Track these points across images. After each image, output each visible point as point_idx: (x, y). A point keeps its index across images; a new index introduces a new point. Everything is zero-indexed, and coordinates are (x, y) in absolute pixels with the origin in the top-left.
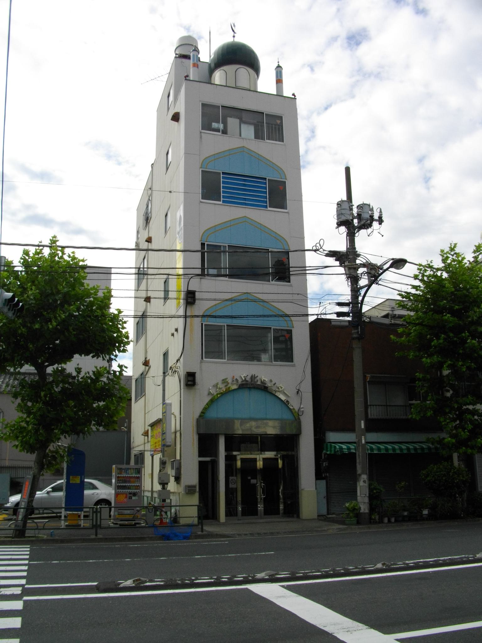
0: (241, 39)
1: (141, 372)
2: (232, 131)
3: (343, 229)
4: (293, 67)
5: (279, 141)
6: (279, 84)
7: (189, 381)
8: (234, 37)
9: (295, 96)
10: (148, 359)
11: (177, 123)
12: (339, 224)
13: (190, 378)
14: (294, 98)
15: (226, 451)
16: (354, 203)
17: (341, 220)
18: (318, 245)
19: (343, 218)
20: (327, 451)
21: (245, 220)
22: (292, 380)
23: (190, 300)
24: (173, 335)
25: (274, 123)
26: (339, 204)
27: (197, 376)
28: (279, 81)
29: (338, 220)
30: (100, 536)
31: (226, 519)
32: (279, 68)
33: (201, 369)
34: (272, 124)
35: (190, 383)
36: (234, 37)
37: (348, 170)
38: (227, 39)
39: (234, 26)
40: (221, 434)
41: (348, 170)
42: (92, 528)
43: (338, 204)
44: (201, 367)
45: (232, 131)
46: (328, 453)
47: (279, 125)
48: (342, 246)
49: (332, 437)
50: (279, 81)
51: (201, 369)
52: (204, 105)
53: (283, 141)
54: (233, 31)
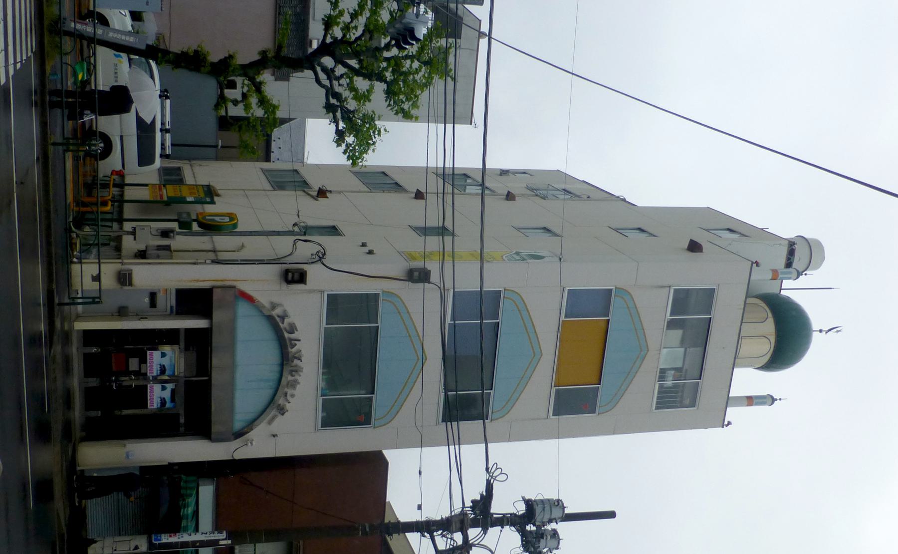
0: (817, 339)
1: (310, 180)
2: (695, 317)
3: (521, 508)
4: (774, 422)
5: (657, 403)
6: (746, 402)
7: (293, 274)
8: (821, 331)
9: (727, 426)
10: (328, 195)
11: (686, 246)
12: (529, 504)
13: (297, 276)
14: (724, 424)
15: (186, 329)
16: (560, 524)
17: (536, 507)
18: (499, 471)
19: (538, 509)
20: (186, 482)
21: (536, 354)
22: (297, 431)
23: (416, 274)
24: (364, 245)
25: (685, 396)
26: (558, 503)
27: (300, 286)
28: (750, 401)
29: (535, 501)
30: (51, 148)
31: (78, 331)
32: (770, 400)
33: (311, 291)
34: (682, 392)
35: (290, 275)
36: (821, 331)
37: (611, 515)
38: (816, 321)
39: (838, 331)
40: (211, 324)
41: (611, 515)
42: (64, 138)
43: (558, 501)
44: (314, 291)
45: (695, 317)
46: (182, 484)
47: (681, 402)
48: (498, 507)
49: (207, 492)
50: (750, 401)
51: (311, 291)
52: (712, 291)
53: (657, 408)
54: (830, 330)
